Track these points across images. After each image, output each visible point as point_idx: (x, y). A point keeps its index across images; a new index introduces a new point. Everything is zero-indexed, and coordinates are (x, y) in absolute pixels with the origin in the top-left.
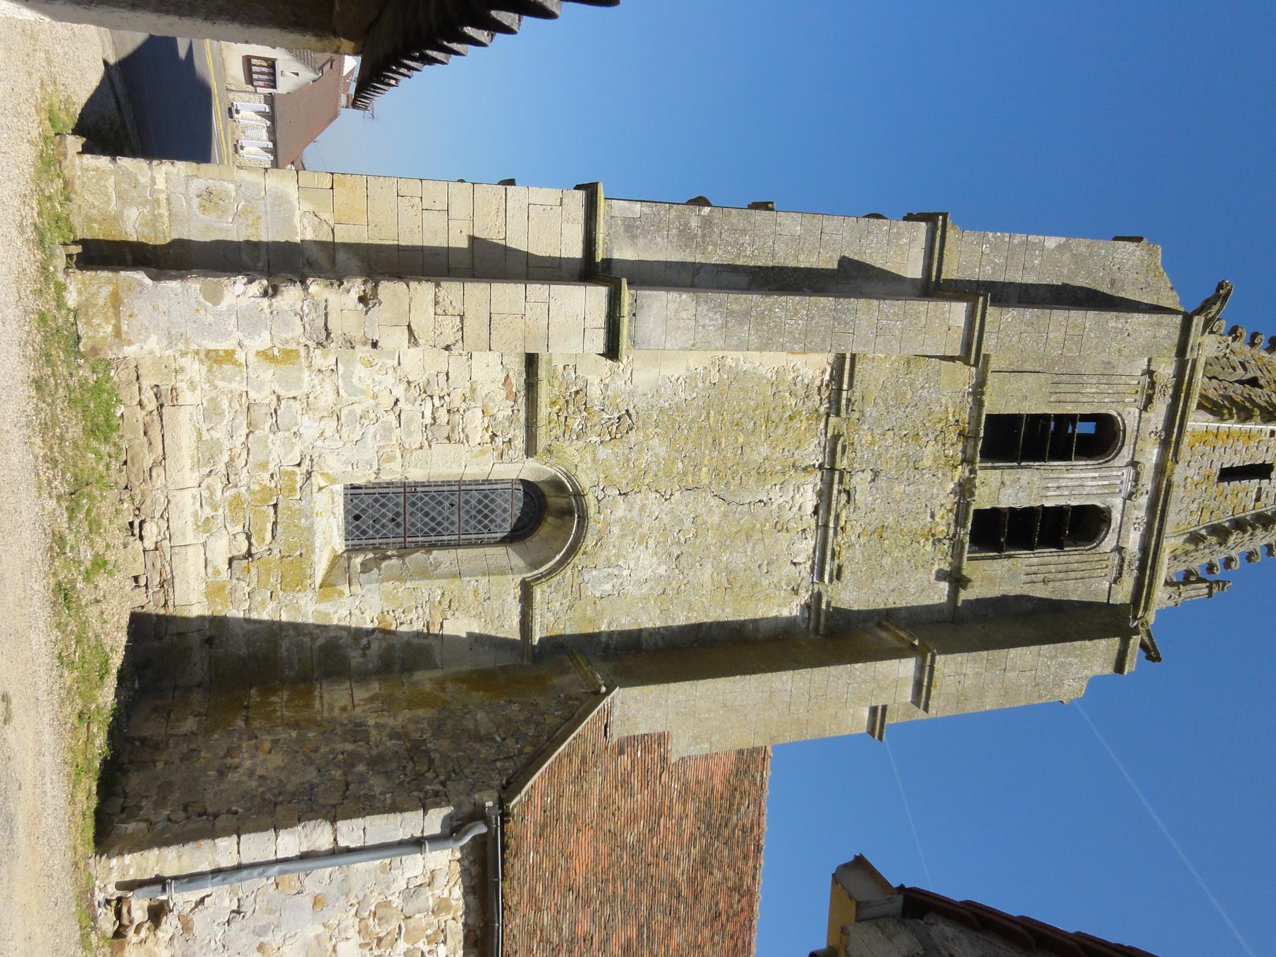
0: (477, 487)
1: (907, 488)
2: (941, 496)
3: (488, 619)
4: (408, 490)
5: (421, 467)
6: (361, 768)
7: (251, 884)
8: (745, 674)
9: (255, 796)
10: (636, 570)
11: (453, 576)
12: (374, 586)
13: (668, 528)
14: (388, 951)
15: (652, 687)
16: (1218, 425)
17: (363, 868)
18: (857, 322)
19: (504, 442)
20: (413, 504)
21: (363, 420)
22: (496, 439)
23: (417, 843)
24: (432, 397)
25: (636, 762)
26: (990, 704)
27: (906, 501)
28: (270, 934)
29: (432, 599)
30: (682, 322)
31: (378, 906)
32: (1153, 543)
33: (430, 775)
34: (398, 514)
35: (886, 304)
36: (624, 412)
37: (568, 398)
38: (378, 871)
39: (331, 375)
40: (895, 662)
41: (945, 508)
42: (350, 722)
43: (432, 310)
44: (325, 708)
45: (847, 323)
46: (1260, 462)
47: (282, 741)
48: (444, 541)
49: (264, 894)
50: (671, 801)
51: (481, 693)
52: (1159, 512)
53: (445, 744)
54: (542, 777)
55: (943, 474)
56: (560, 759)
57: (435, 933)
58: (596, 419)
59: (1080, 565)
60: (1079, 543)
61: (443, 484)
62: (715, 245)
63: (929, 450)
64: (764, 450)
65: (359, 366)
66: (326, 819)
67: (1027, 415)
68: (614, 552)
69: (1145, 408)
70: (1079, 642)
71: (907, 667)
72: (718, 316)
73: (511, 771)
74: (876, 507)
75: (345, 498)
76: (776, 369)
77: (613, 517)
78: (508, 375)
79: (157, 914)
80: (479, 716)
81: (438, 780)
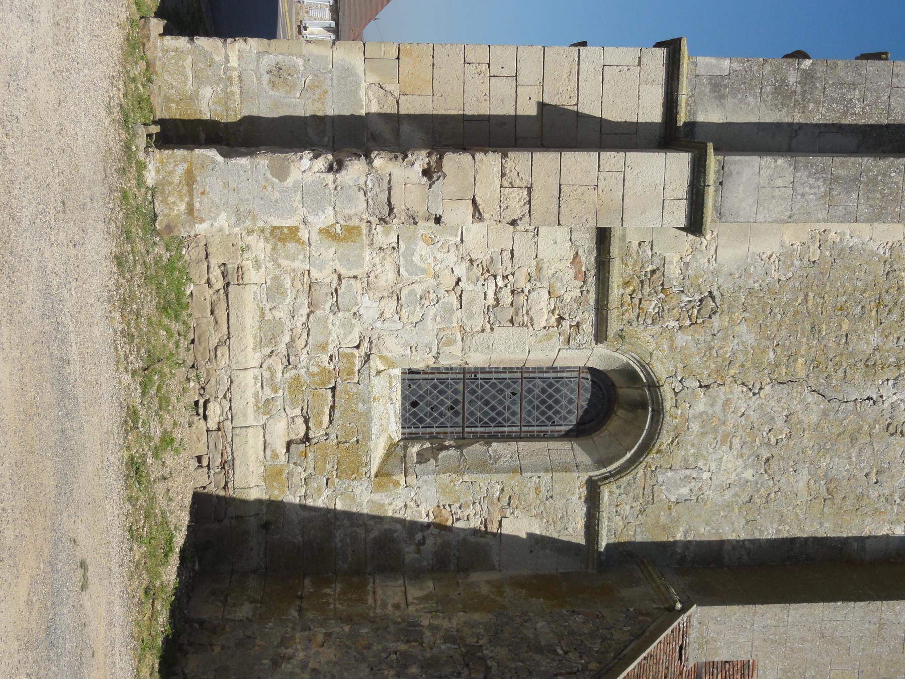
0: (541, 375)
3: (551, 520)
4: (467, 376)
10: (719, 472)
12: (431, 477)
13: (756, 427)
15: (735, 608)
19: (571, 326)
20: (473, 392)
22: (563, 323)
24: (495, 277)
29: (490, 494)
34: (456, 402)
36: (706, 294)
37: (643, 278)
39: (392, 253)
48: (477, 433)
53: (502, 652)
58: (674, 302)
61: (505, 370)
62: (817, 103)
64: (875, 339)
65: (421, 243)
68: (692, 451)
72: (820, 183)
75: (402, 383)
76: (890, 244)
77: (692, 411)
78: (577, 253)
80: (539, 625)
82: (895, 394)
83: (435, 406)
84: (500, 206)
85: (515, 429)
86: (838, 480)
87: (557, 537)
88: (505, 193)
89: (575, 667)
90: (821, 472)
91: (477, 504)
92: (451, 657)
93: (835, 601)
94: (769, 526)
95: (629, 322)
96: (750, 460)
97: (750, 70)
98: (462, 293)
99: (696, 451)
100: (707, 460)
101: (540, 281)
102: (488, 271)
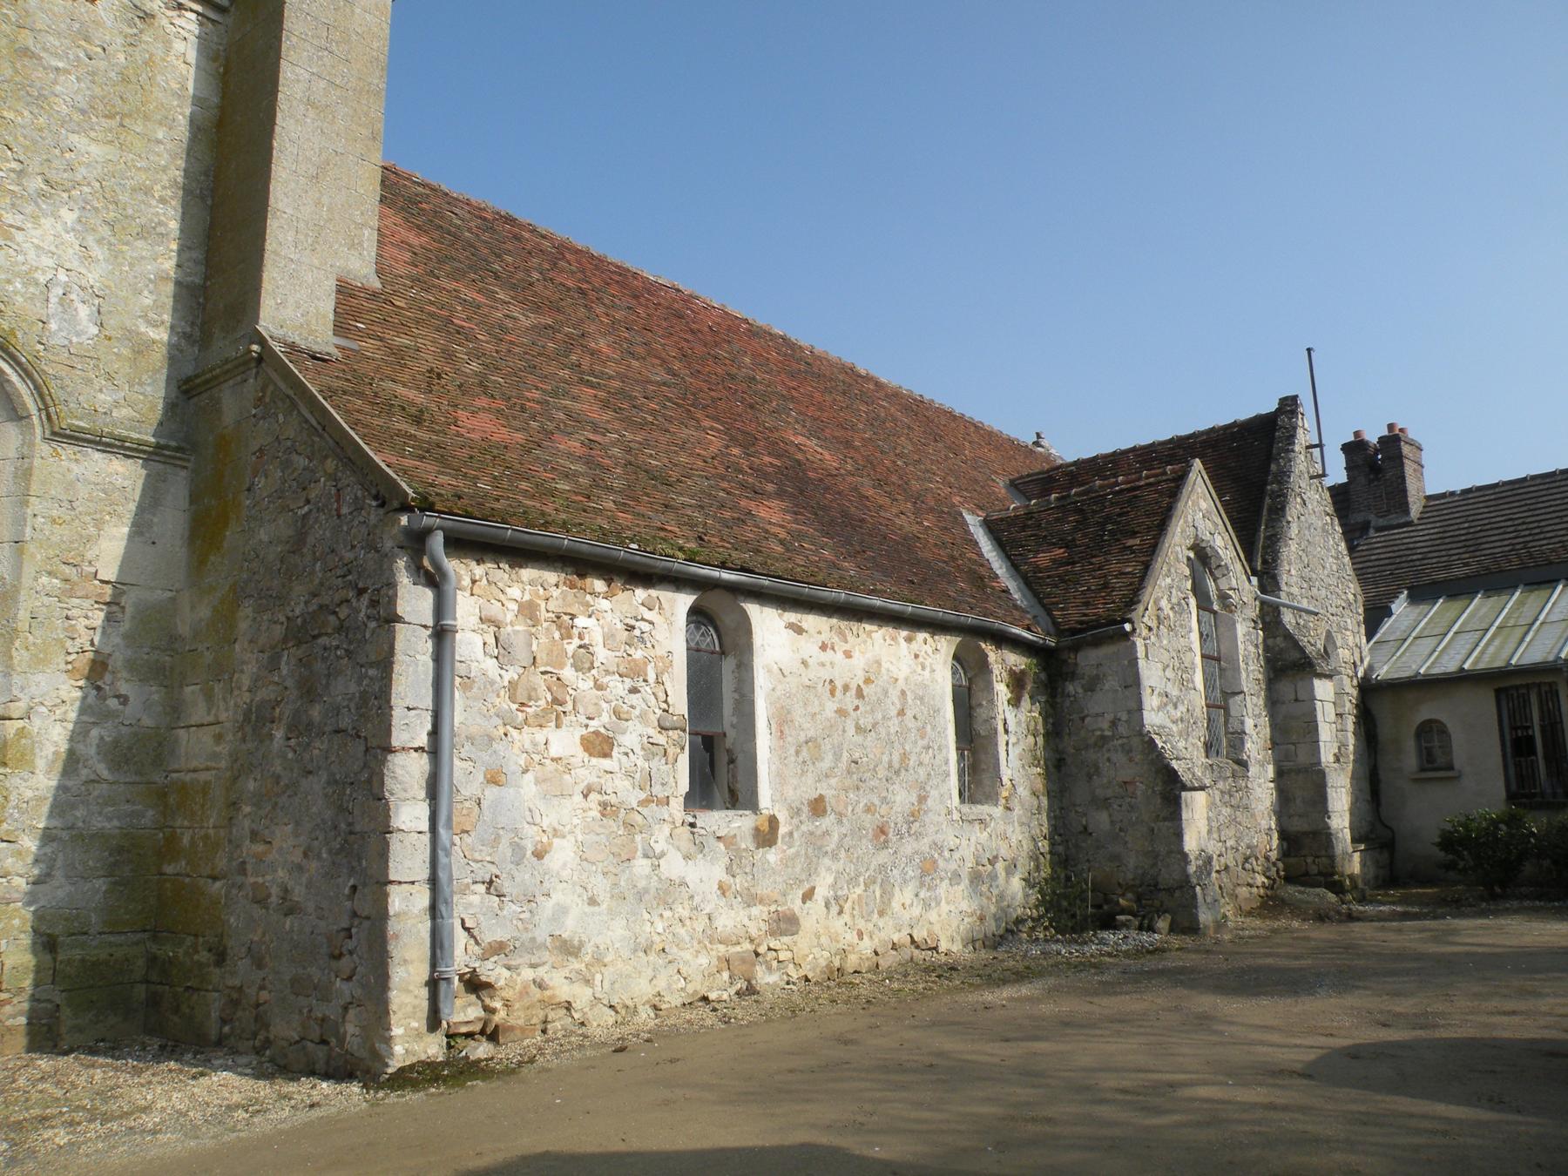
3: (108, 509)
6: (316, 712)
7: (458, 868)
8: (272, 131)
9: (334, 863)
14: (571, 692)
15: (265, 276)
17: (461, 713)
23: (441, 634)
28: (523, 843)
29: (57, 592)
31: (512, 699)
33: (344, 612)
38: (468, 694)
42: (241, 728)
44: (213, 764)
47: (254, 826)
49: (473, 849)
50: (432, 303)
54: (377, 451)
56: (355, 424)
57: (559, 627)
66: (383, 762)
68: (19, 286)
79: (475, 985)
81: (354, 601)
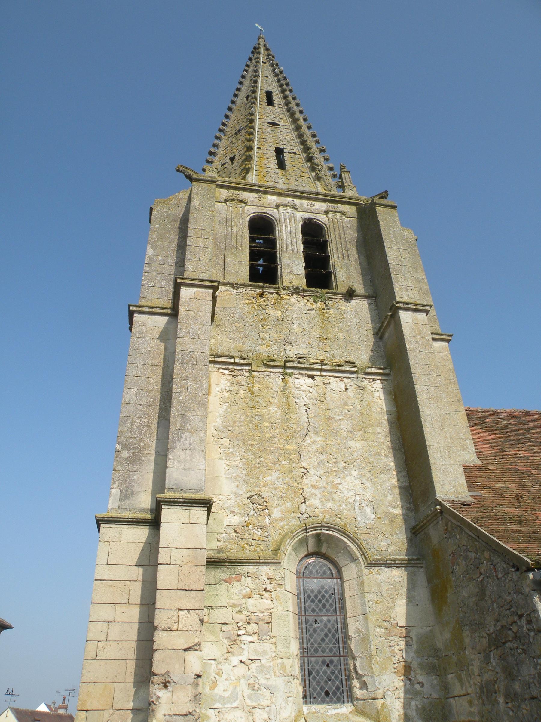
0: (303, 604)
1: (295, 325)
2: (300, 305)
3: (395, 592)
4: (306, 655)
5: (289, 644)
6: (517, 686)
10: (355, 490)
11: (366, 619)
12: (376, 679)
13: (327, 470)
15: (434, 475)
16: (254, 171)
18: (190, 350)
19: (271, 583)
20: (316, 650)
21: (256, 688)
22: (268, 589)
24: (239, 635)
25: (484, 485)
26: (422, 276)
27: (303, 325)
29: (384, 635)
30: (187, 458)
32: (321, 197)
34: (323, 662)
35: (180, 334)
36: (249, 500)
37: (240, 538)
39: (222, 713)
40: (403, 325)
41: (306, 303)
42: (480, 697)
43: (174, 633)
45: (191, 357)
46: (274, 153)
48: (341, 627)
50: (506, 463)
51: (448, 595)
52: (304, 195)
53: (489, 619)
54: (507, 543)
55: (286, 305)
58: (254, 519)
59: (336, 232)
60: (324, 234)
61: (300, 628)
62: (140, 441)
63: (271, 312)
64: (273, 409)
65: (216, 691)
67: (250, 260)
68: (344, 506)
69: (245, 203)
70: (381, 228)
71: (405, 317)
72: (184, 435)
73: (505, 566)
74: (307, 341)
75: (313, 703)
76: (221, 403)
77: (320, 507)
78: (223, 580)
80: (465, 595)
81: (518, 622)
82: (303, 398)
83: (327, 678)
84: (190, 631)
85: (339, 620)
86: (353, 425)
87: (406, 588)
88: (181, 627)
89: (490, 567)
90: (350, 435)
91: (391, 644)
92: (500, 656)
93: (421, 422)
94: (383, 461)
95: (267, 547)
96: (346, 473)
97: (118, 477)
98: (250, 659)
99: (344, 504)
100: (349, 497)
101: (242, 605)
102: (235, 641)
